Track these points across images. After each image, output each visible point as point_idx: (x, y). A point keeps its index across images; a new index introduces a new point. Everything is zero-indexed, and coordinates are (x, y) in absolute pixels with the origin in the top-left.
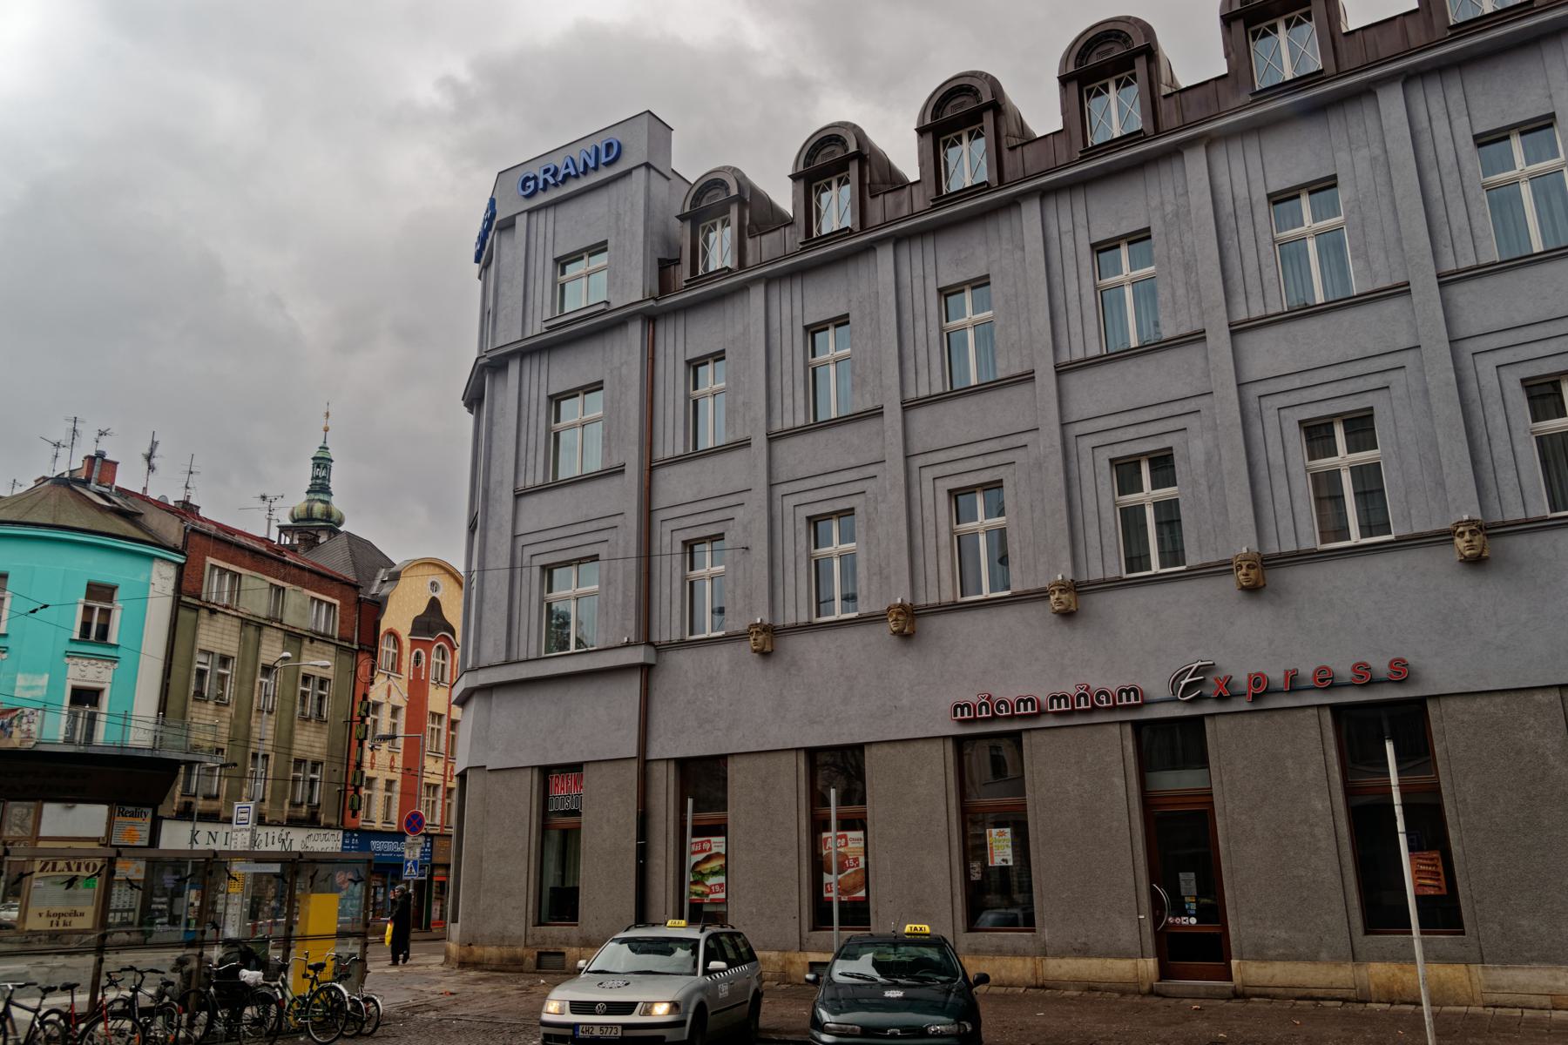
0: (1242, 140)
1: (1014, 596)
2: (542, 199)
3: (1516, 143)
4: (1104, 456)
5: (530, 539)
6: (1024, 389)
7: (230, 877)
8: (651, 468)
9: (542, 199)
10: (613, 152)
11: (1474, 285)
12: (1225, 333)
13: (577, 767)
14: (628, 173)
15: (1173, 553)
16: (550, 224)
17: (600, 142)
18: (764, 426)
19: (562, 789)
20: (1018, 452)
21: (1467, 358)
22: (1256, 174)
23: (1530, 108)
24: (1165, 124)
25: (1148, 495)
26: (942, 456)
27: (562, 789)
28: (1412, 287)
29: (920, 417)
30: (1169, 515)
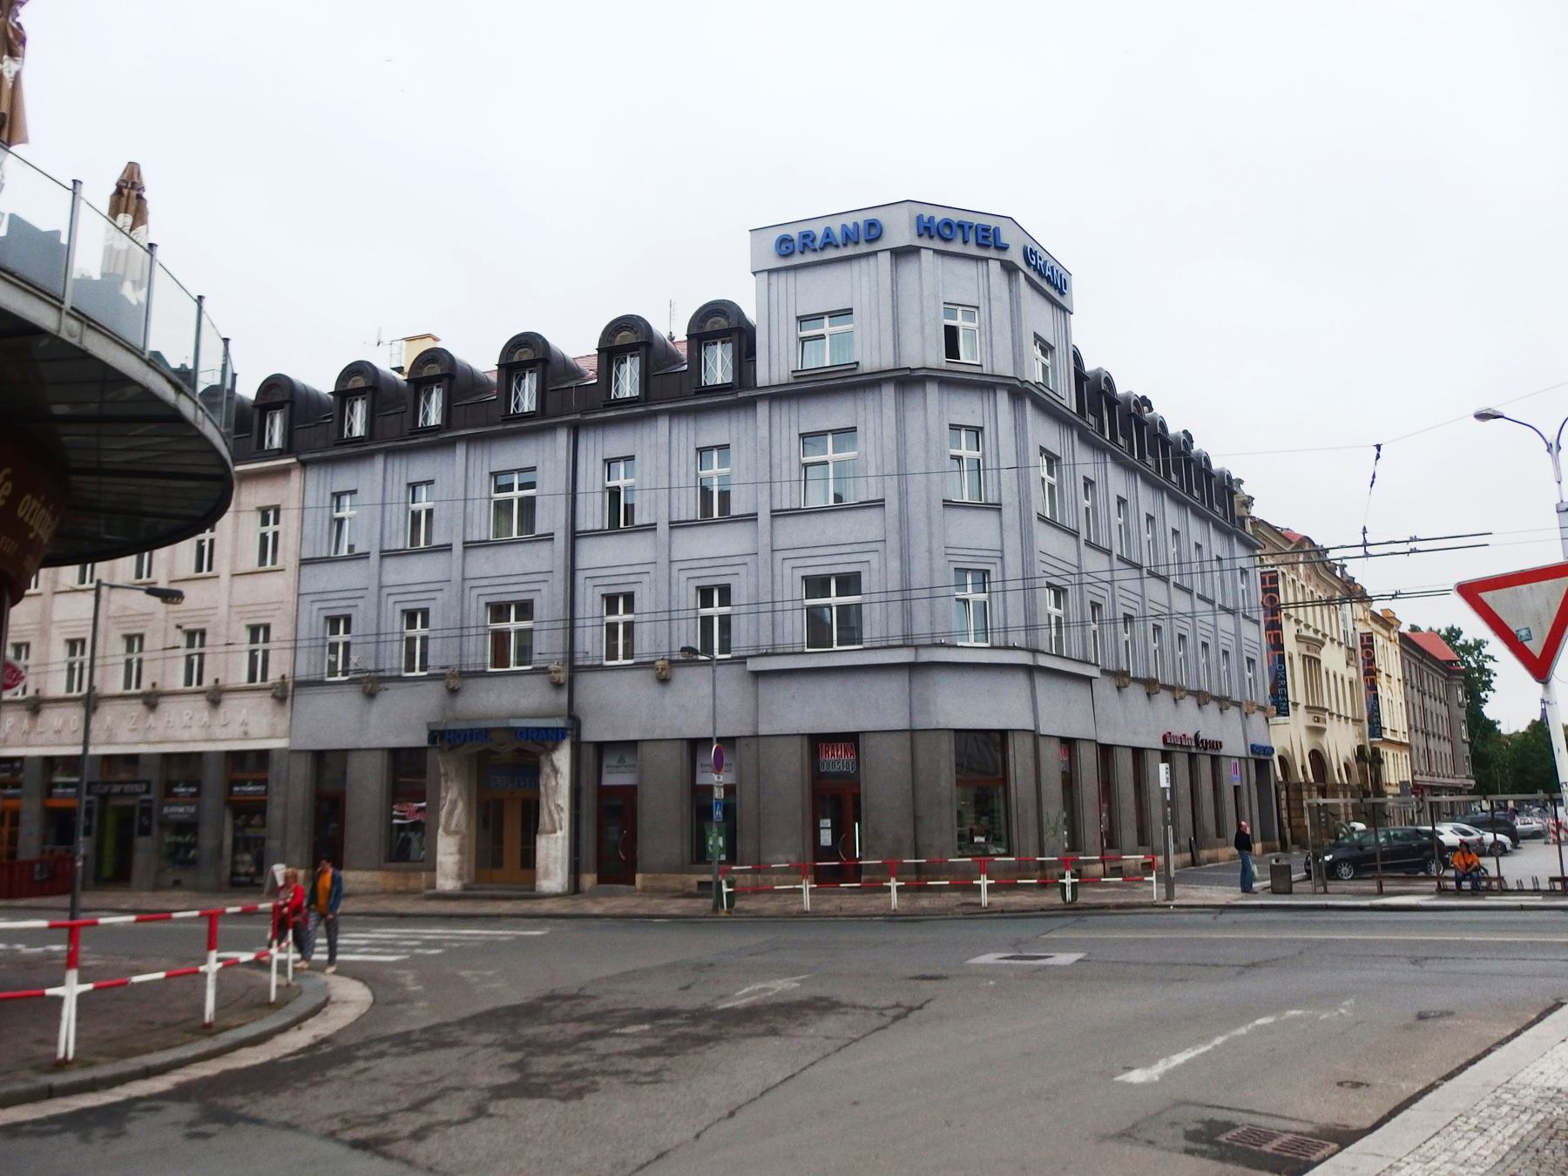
0: (575, 430)
1: (733, 658)
2: (797, 260)
3: (830, 438)
4: (399, 608)
5: (476, 583)
6: (649, 535)
7: (1386, 817)
8: (574, 535)
9: (797, 260)
10: (873, 230)
11: (790, 520)
12: (461, 547)
13: (632, 745)
14: (875, 253)
15: (725, 648)
16: (791, 290)
17: (860, 219)
18: (378, 545)
19: (833, 755)
20: (359, 600)
21: (675, 573)
22: (404, 475)
23: (844, 422)
24: (549, 408)
25: (513, 625)
26: (485, 582)
27: (833, 755)
28: (886, 503)
29: (390, 563)
30: (725, 621)
